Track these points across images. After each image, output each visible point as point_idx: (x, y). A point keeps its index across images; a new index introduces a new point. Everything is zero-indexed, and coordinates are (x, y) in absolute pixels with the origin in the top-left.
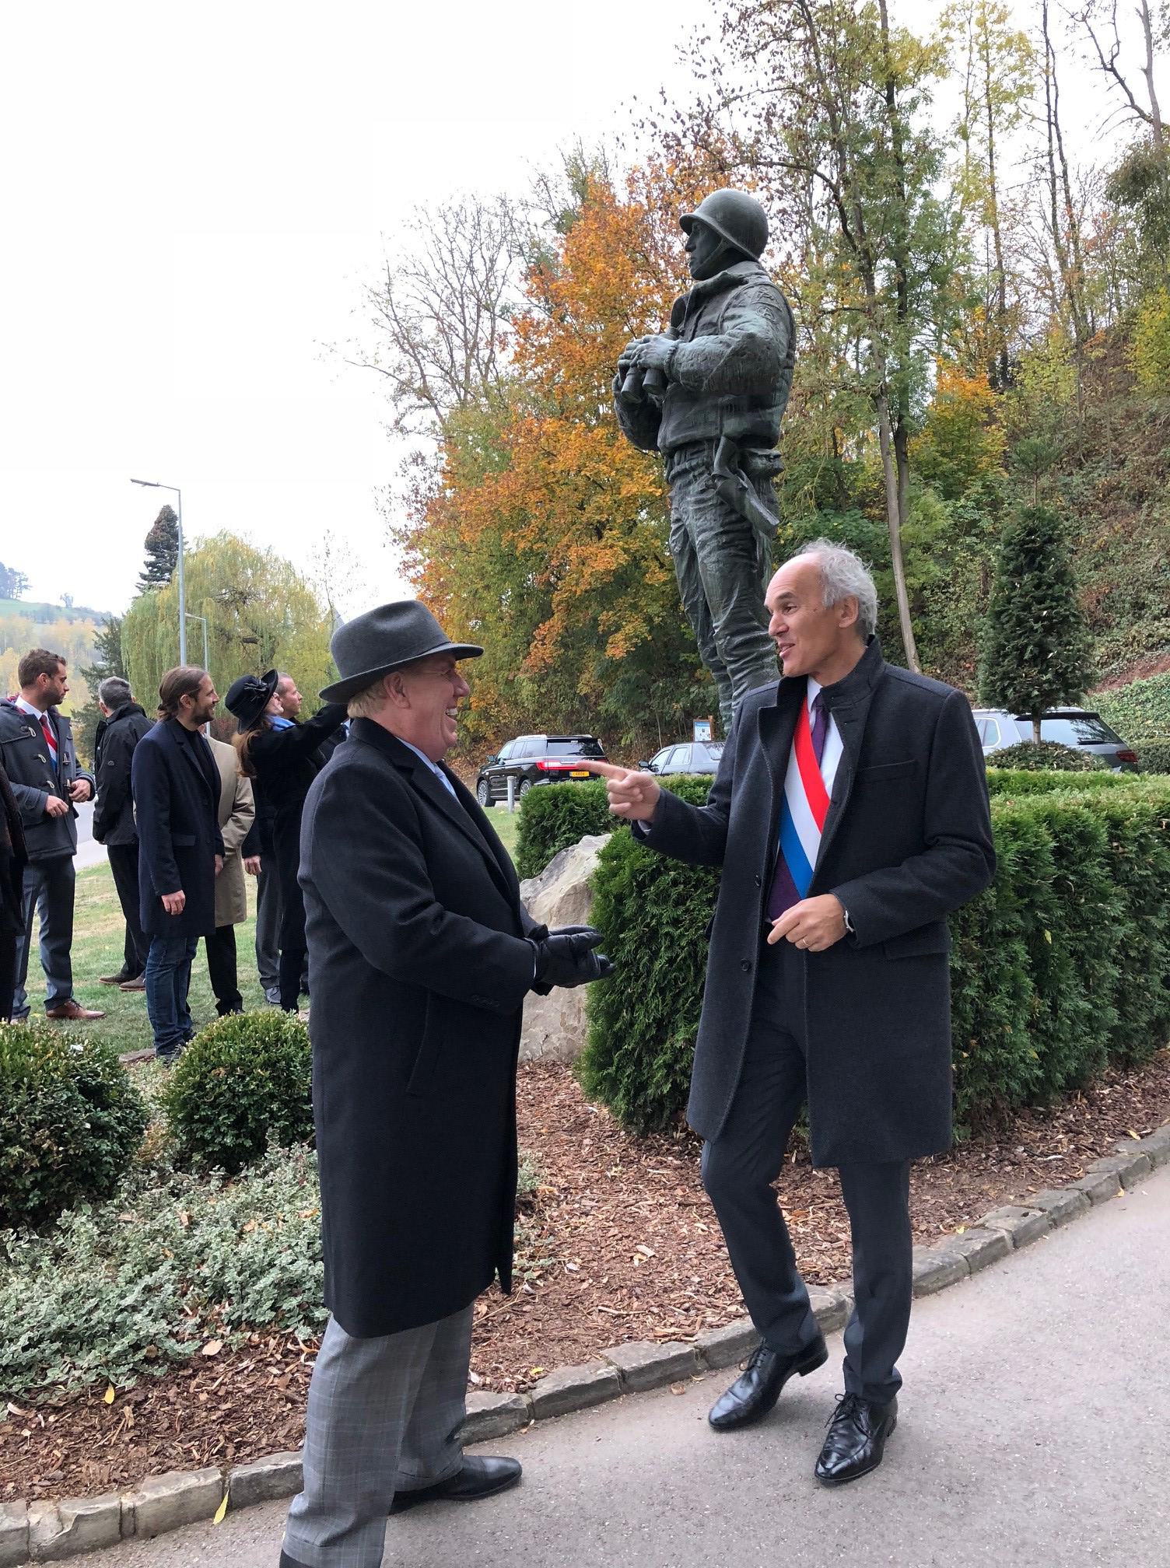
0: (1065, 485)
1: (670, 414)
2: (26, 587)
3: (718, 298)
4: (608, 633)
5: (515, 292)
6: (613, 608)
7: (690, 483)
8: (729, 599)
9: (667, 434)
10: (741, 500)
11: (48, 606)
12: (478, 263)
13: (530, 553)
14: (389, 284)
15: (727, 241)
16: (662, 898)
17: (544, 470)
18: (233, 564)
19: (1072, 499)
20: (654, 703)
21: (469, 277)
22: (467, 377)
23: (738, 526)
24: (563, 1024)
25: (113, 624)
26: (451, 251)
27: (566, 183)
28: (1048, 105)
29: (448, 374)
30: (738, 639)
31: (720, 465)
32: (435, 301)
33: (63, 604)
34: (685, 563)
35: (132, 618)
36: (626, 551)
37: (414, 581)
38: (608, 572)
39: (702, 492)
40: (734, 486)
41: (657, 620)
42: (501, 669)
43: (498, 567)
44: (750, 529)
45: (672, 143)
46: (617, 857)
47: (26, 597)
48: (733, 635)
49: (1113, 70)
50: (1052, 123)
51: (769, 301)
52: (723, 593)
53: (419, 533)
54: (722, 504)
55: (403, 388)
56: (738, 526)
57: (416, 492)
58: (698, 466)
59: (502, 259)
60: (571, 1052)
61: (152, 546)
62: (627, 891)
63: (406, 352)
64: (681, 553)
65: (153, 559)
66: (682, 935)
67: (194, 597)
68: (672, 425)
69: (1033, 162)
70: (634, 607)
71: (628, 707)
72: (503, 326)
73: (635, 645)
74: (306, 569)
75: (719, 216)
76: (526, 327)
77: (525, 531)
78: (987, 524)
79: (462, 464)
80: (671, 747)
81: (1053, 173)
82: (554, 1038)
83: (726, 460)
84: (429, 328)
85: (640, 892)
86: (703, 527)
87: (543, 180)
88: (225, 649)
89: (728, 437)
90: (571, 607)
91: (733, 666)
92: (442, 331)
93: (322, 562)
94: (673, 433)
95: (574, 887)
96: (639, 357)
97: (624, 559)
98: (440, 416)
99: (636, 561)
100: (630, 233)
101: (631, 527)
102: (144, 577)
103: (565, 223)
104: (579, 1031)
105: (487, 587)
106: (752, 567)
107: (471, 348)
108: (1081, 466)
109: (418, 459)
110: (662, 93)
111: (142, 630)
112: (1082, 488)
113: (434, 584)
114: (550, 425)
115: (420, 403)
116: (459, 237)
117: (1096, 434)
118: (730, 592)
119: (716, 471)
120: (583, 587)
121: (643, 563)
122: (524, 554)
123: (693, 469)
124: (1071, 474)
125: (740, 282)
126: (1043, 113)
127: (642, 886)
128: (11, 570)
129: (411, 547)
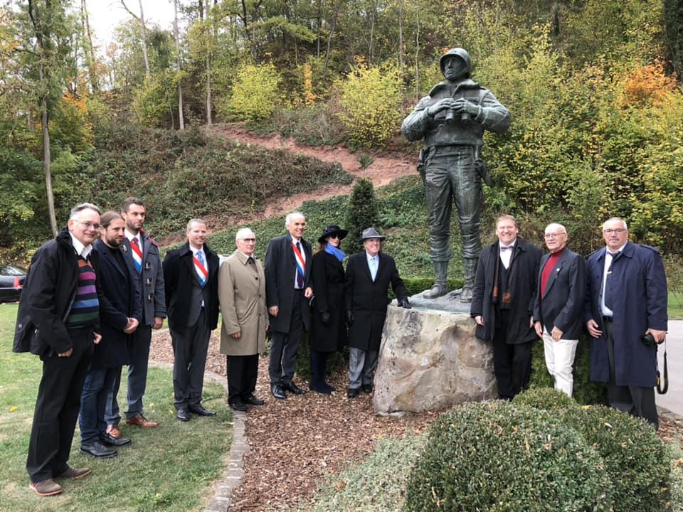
34: (441, 192)
64: (441, 187)
82: (438, 397)
95: (448, 328)
112: (130, 160)
123: (461, 155)
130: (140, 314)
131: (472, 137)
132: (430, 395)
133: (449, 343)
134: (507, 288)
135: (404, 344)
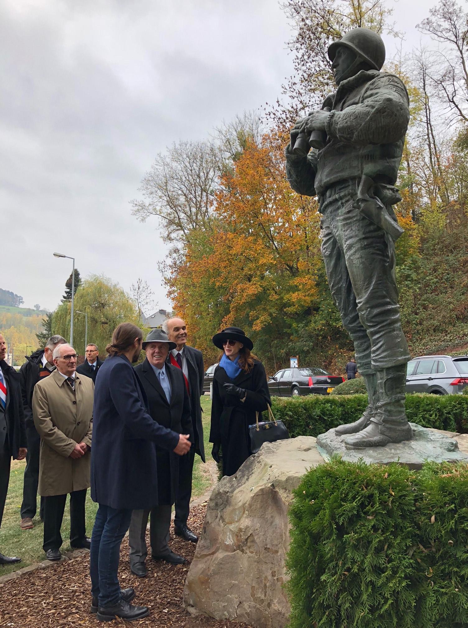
0: (446, 260)
1: (324, 166)
2: (21, 302)
3: (357, 90)
4: (253, 320)
5: (216, 184)
6: (255, 310)
7: (338, 208)
8: (369, 284)
9: (322, 178)
10: (379, 216)
11: (29, 309)
12: (202, 174)
13: (221, 287)
14: (166, 183)
15: (361, 56)
16: (363, 544)
17: (227, 253)
18: (99, 292)
19: (450, 266)
20: (273, 350)
21: (198, 180)
22: (197, 218)
23: (375, 234)
24: (253, 595)
25: (50, 316)
26: (191, 170)
27: (237, 143)
28: (427, 117)
29: (189, 217)
30: (376, 311)
31: (362, 193)
32: (184, 189)
33: (35, 309)
34: (333, 262)
35: (57, 313)
36: (261, 286)
37: (173, 299)
38: (254, 295)
39: (349, 212)
40: (374, 206)
41: (274, 315)
42: (208, 335)
43: (208, 293)
44: (383, 236)
45: (282, 123)
46: (314, 496)
47: (21, 306)
48: (372, 307)
49: (453, 102)
50: (428, 122)
51: (396, 84)
52: (364, 281)
53: (175, 279)
54: (364, 219)
55: (171, 222)
56: (375, 234)
57: (175, 264)
58: (345, 196)
59: (211, 174)
60: (259, 620)
61: (69, 285)
62: (326, 533)
63: (172, 208)
64: (330, 256)
65: (68, 290)
66: (385, 584)
67: (83, 305)
68: (326, 171)
69: (422, 137)
70: (264, 309)
71: (261, 351)
72: (211, 198)
73: (265, 325)
74: (131, 294)
75: (356, 41)
76: (220, 197)
77: (219, 279)
78: (414, 276)
79: (194, 252)
80: (283, 370)
81: (429, 142)
82: (246, 605)
83: (367, 189)
84: (182, 199)
85: (340, 536)
86: (349, 238)
87: (228, 140)
88: (94, 326)
89: (366, 174)
90: (238, 309)
91: (372, 330)
92: (187, 201)
93: (136, 292)
94: (327, 176)
95: (262, 490)
96: (307, 124)
97: (260, 289)
98: (185, 233)
99: (265, 290)
100: (263, 160)
101: (262, 277)
102: (64, 297)
103: (236, 157)
104: (266, 603)
105: (203, 301)
106: (385, 261)
107: (199, 208)
108: (452, 252)
109: (176, 251)
110: (278, 102)
111: (61, 318)
112: (454, 261)
113: (181, 300)
114: (230, 235)
115: (177, 228)
116: (194, 164)
117: (457, 240)
118: (371, 278)
119: (359, 195)
120: (243, 301)
121: (268, 292)
122: (219, 288)
123: (341, 198)
124: (448, 256)
125: (373, 77)
126: (424, 119)
127: (342, 531)
128: (16, 295)
129: (172, 285)
130: (192, 429)
131: (355, 163)
132: (234, 597)
133: (268, 516)
134: (390, 429)
135: (217, 504)
